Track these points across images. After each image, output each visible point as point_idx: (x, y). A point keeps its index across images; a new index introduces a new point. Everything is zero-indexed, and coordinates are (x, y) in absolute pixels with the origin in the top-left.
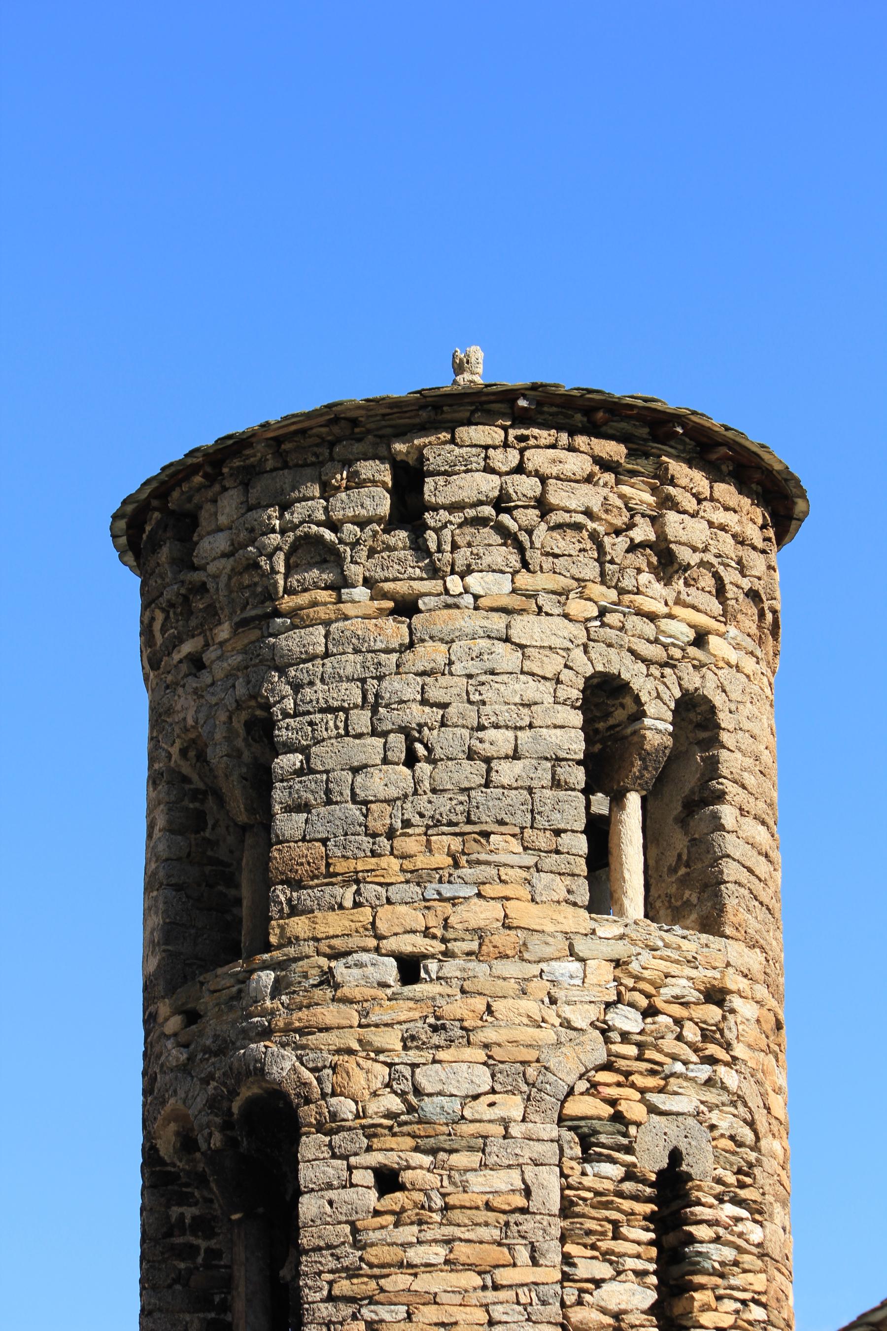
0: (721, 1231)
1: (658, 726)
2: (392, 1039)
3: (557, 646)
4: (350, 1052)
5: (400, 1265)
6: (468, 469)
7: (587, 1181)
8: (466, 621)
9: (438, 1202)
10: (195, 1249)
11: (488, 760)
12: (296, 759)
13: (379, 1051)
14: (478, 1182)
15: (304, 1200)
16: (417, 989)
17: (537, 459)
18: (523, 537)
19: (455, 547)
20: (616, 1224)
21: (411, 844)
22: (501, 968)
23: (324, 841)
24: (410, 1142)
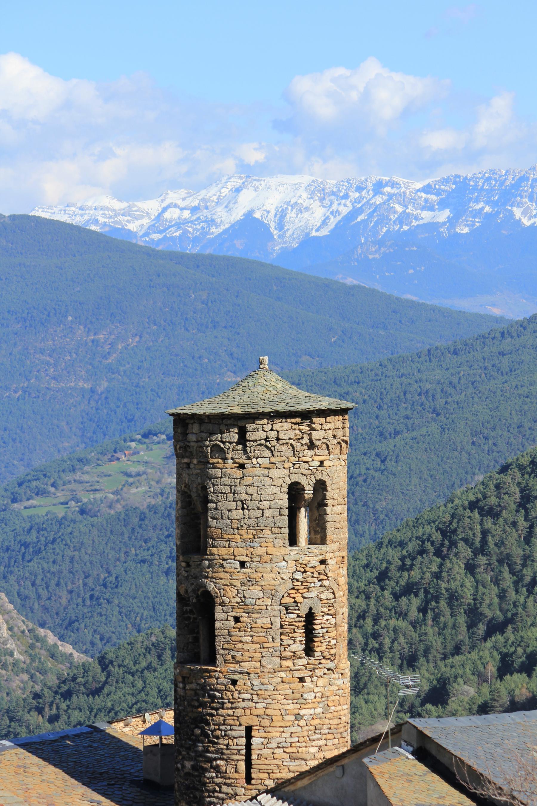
0: (322, 625)
1: (309, 492)
2: (238, 583)
3: (282, 477)
4: (227, 585)
5: (240, 642)
6: (257, 431)
7: (287, 620)
8: (258, 471)
9: (249, 626)
10: (190, 618)
11: (263, 510)
13: (235, 586)
14: (259, 621)
15: (216, 623)
16: (245, 570)
17: (276, 427)
18: (273, 448)
19: (254, 451)
20: (294, 629)
21: (242, 532)
23: (221, 529)
24: (242, 610)
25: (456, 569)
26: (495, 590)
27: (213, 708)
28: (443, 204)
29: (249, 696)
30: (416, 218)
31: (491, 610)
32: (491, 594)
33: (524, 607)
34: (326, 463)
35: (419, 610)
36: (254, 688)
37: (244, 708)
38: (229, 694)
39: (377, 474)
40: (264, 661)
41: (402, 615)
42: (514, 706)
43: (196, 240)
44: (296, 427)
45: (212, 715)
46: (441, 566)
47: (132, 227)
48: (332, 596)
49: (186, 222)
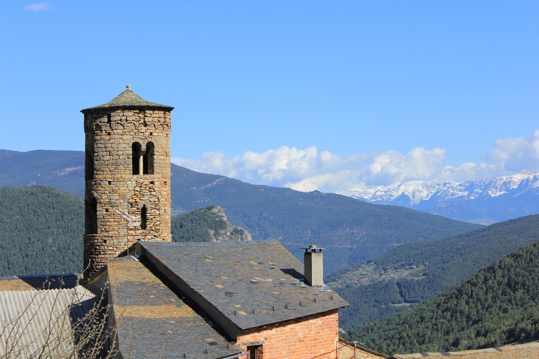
1: (144, 147)
2: (107, 192)
8: (117, 136)
12: (97, 154)
17: (125, 114)
21: (109, 167)
22: (121, 183)
25: (462, 303)
26: (475, 310)
27: (96, 255)
28: (466, 190)
29: (112, 248)
30: (457, 194)
31: (474, 317)
32: (474, 312)
33: (485, 315)
34: (153, 134)
35: (450, 316)
36: (115, 244)
37: (109, 254)
38: (103, 247)
39: (442, 275)
40: (120, 231)
41: (445, 318)
42: (480, 347)
43: (386, 201)
44: (137, 114)
45: (95, 258)
46: (457, 302)
47: (366, 197)
48: (157, 200)
49: (383, 196)
